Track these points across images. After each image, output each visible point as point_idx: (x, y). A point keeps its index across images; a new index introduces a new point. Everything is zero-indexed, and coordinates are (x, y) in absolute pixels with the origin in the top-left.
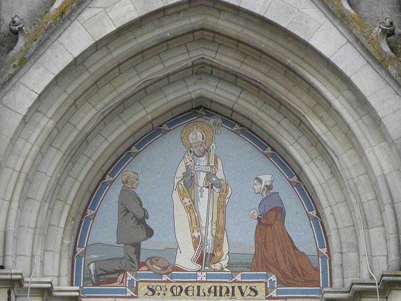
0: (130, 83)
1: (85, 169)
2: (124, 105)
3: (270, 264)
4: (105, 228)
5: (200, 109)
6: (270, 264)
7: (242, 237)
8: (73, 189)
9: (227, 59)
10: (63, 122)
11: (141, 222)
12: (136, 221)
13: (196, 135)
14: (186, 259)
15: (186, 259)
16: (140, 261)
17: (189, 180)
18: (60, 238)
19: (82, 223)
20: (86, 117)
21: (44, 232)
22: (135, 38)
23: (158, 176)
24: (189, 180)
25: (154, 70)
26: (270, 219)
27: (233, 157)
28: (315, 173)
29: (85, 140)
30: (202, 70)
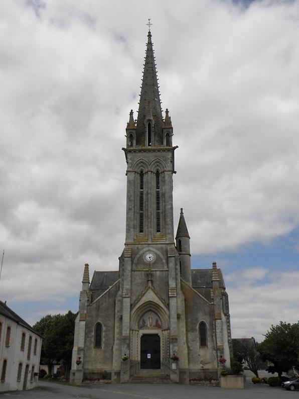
0: (143, 309)
1: (139, 317)
2: (143, 311)
3: (213, 340)
4: (141, 323)
5: (150, 310)
6: (213, 340)
7: (154, 323)
8: (138, 319)
9: (152, 306)
10: (137, 312)
11: (144, 322)
12: (144, 322)
13: (150, 313)
14: (149, 326)
15: (149, 326)
16: (178, 381)
17: (149, 318)
18: (137, 324)
19: (139, 322)
20: (139, 312)
21: (135, 324)
22: (158, 174)
23: (146, 317)
24: (149, 318)
25: (145, 307)
26: (157, 321)
27: (153, 315)
28: (161, 317)
29: (139, 314)
30: (150, 307)
